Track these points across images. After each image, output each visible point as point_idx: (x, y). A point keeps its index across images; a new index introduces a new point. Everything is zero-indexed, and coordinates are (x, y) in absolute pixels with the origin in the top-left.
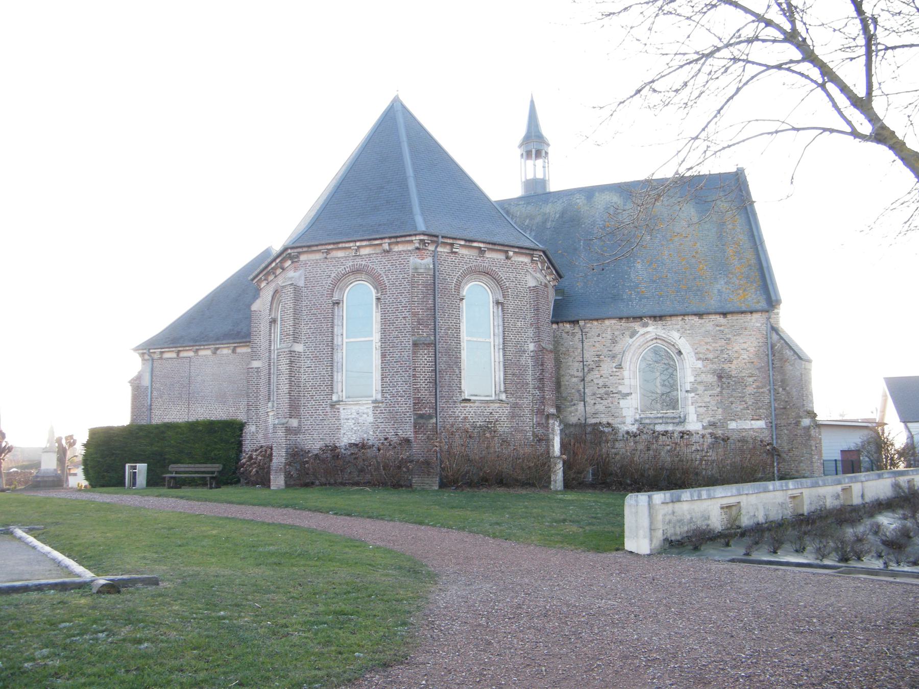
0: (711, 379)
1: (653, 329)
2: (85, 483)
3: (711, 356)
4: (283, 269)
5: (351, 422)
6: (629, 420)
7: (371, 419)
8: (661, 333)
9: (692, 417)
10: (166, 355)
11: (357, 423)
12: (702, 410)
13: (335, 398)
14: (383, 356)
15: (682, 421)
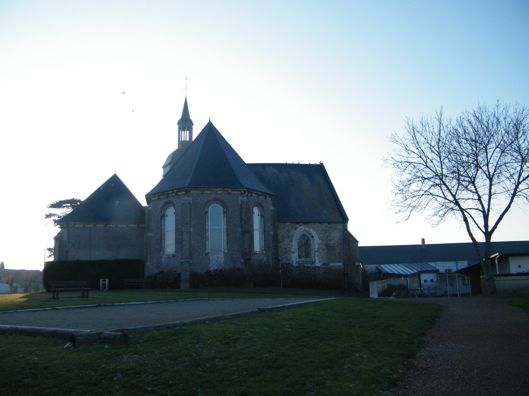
0: (324, 247)
1: (302, 228)
2: (44, 290)
3: (324, 238)
4: (176, 195)
5: (214, 261)
6: (294, 262)
7: (223, 260)
8: (307, 229)
9: (317, 261)
10: (77, 226)
11: (217, 261)
12: (321, 259)
13: (207, 251)
14: (228, 235)
15: (314, 262)
